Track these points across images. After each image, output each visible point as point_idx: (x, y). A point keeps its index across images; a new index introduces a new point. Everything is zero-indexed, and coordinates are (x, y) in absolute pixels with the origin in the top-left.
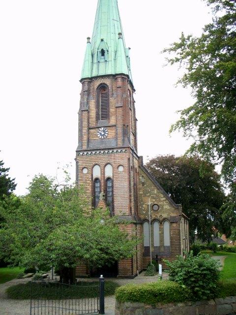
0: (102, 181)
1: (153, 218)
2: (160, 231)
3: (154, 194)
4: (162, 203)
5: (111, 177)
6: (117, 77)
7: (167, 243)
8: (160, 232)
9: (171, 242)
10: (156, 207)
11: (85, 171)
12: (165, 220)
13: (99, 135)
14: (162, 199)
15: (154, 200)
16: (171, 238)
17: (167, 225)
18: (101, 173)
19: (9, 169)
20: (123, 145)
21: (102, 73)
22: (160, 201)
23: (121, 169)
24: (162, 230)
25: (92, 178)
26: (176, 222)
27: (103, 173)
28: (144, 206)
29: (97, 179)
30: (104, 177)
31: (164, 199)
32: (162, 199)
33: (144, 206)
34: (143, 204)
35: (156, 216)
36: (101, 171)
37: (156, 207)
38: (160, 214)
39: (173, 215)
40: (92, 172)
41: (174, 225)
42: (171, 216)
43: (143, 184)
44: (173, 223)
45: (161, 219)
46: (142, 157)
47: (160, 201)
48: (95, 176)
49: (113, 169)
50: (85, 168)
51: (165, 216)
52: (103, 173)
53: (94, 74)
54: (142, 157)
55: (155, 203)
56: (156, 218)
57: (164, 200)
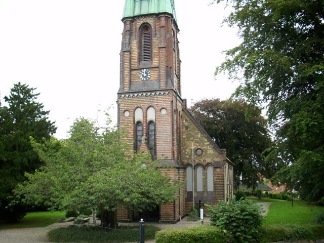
0: (145, 125)
1: (196, 163)
2: (203, 176)
3: (198, 138)
4: (206, 147)
5: (154, 120)
6: (160, 16)
7: (210, 188)
8: (204, 177)
9: (215, 188)
10: (199, 152)
11: (127, 114)
12: (208, 164)
13: (141, 77)
14: (206, 144)
15: (198, 144)
16: (215, 184)
17: (210, 170)
18: (143, 116)
19: (49, 111)
20: (166, 87)
21: (144, 12)
22: (204, 145)
23: (164, 112)
24: (205, 175)
25: (134, 123)
26: (220, 167)
27: (145, 116)
28: (187, 150)
29: (139, 122)
30: (146, 120)
31: (208, 143)
32: (206, 144)
33: (187, 150)
34: (186, 148)
35: (200, 161)
36: (143, 114)
37: (199, 152)
38: (203, 159)
39: (217, 160)
40: (134, 115)
41: (218, 170)
42: (214, 161)
43: (187, 128)
44: (217, 168)
45: (204, 164)
46: (186, 100)
47: (204, 145)
48: (136, 120)
49: (156, 112)
50: (127, 110)
51: (208, 160)
52: (145, 116)
53: (137, 13)
54: (186, 100)
55: (199, 147)
56: (200, 162)
57: (208, 145)
